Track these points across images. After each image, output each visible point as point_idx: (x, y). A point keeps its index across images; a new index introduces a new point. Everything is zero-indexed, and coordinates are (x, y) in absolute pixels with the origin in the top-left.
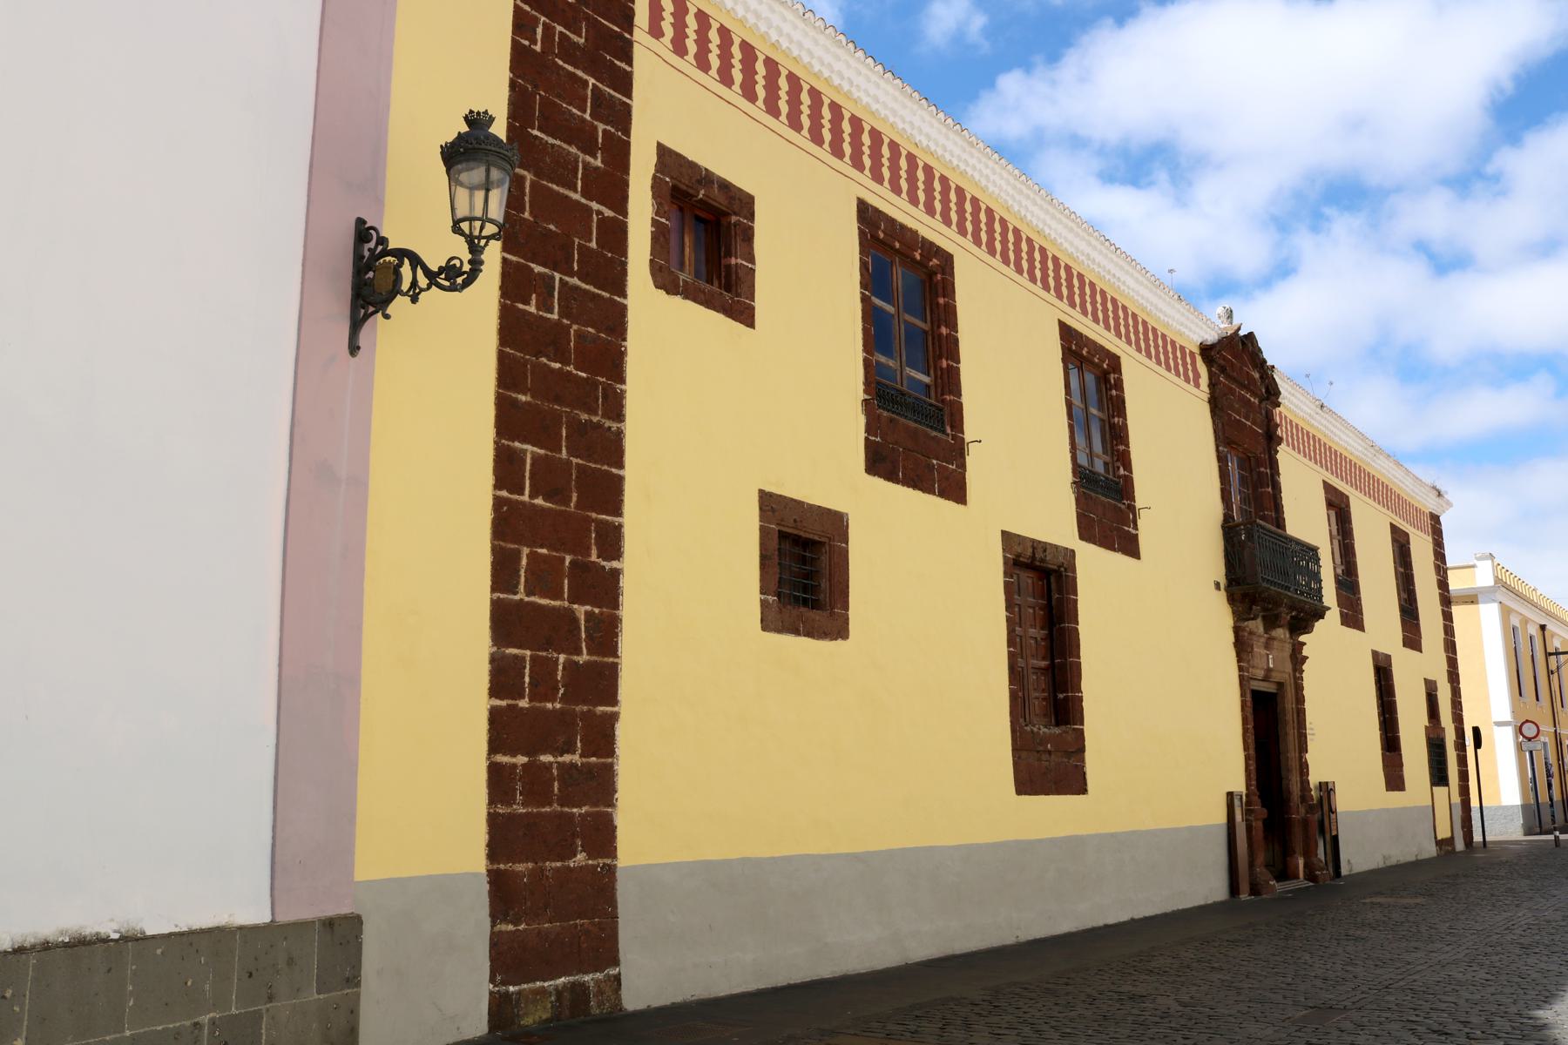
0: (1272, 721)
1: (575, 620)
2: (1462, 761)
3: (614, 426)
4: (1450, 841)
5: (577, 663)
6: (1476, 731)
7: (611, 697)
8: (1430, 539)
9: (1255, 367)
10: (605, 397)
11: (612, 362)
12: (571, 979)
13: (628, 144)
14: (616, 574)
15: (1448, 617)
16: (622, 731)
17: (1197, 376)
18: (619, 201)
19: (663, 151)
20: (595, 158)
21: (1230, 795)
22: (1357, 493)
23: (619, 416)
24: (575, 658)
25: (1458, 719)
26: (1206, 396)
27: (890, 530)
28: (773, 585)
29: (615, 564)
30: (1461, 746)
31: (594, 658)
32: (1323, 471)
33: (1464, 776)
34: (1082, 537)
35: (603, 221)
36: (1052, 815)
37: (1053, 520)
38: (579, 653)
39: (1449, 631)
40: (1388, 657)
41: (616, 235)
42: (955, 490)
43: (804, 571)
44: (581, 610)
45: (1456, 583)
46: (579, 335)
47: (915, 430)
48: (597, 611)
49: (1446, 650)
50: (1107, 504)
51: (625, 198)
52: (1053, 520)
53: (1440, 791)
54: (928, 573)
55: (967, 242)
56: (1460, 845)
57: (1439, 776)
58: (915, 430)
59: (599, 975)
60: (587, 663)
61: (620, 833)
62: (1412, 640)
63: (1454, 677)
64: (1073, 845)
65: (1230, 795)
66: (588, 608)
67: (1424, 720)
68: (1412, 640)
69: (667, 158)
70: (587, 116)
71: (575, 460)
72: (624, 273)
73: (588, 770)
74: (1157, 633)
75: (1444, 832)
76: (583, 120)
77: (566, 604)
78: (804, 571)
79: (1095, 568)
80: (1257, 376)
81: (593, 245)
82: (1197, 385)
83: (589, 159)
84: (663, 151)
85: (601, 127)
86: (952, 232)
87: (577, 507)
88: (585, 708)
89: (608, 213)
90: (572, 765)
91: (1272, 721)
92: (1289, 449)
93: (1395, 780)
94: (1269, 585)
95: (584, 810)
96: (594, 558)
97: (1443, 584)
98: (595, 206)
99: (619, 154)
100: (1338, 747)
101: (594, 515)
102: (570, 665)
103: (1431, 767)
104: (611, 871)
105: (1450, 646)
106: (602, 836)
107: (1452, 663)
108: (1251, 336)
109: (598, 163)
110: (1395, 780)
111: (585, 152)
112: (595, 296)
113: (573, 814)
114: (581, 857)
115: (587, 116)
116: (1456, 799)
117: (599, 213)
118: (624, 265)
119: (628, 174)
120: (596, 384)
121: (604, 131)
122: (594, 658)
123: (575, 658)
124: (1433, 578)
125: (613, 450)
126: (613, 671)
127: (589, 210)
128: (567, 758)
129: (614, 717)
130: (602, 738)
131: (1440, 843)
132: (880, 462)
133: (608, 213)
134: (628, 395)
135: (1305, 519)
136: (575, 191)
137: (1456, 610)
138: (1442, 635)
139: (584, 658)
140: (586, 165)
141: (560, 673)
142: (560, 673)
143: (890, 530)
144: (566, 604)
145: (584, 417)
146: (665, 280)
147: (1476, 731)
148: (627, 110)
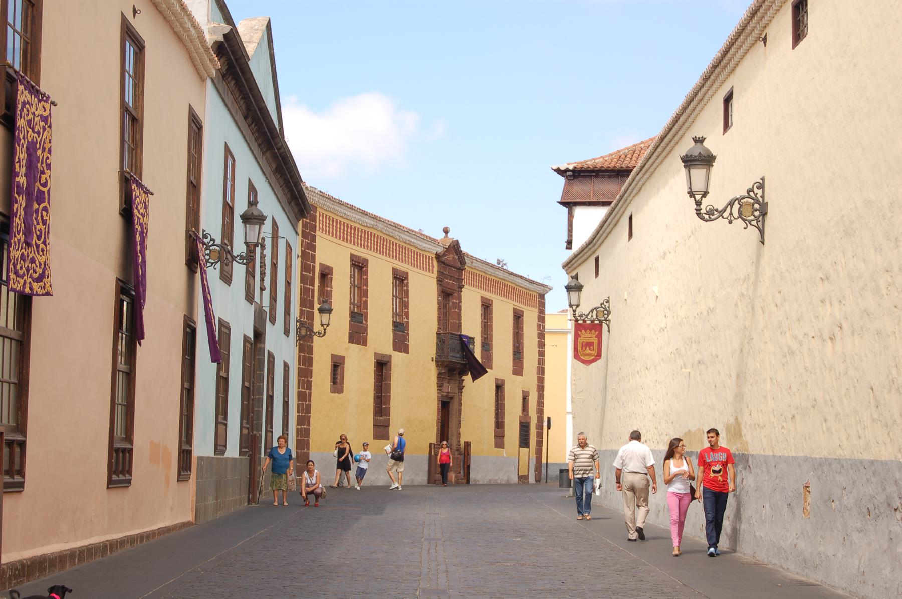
2: (540, 435)
6: (549, 419)
9: (457, 254)
15: (542, 345)
17: (433, 267)
21: (431, 444)
25: (540, 412)
26: (435, 275)
30: (540, 427)
32: (479, 291)
33: (539, 444)
37: (386, 348)
39: (541, 362)
40: (503, 381)
45: (549, 325)
49: (538, 373)
50: (401, 342)
52: (386, 348)
53: (524, 451)
56: (532, 480)
57: (524, 442)
62: (518, 370)
63: (541, 388)
65: (431, 444)
68: (518, 370)
69: (321, 264)
75: (523, 472)
79: (398, 359)
91: (448, 409)
103: (520, 438)
105: (541, 371)
107: (541, 381)
116: (533, 457)
124: (535, 332)
137: (548, 339)
138: (536, 365)
147: (549, 419)
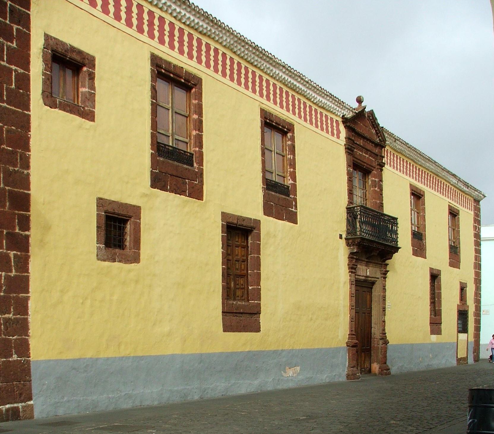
0: (365, 297)
1: (10, 258)
3: (26, 172)
4: (465, 359)
5: (10, 276)
7: (26, 290)
8: (472, 213)
10: (21, 159)
11: (23, 142)
12: (12, 405)
13: (29, 35)
14: (27, 237)
16: (31, 304)
17: (339, 132)
18: (25, 63)
19: (47, 37)
20: (12, 43)
22: (430, 190)
23: (28, 167)
24: (10, 274)
27: (163, 216)
28: (103, 239)
29: (27, 233)
31: (18, 274)
34: (265, 214)
35: (18, 75)
36: (241, 341)
37: (250, 204)
38: (11, 272)
41: (24, 81)
42: (197, 193)
43: (117, 230)
44: (12, 254)
46: (8, 131)
47: (177, 167)
48: (19, 253)
50: (280, 197)
51: (28, 63)
52: (250, 204)
53: (463, 336)
54: (181, 237)
55: (211, 72)
56: (471, 360)
57: (463, 328)
58: (177, 167)
59: (23, 404)
60: (15, 276)
61: (31, 347)
63: (478, 281)
64: (253, 356)
66: (15, 252)
67: (457, 301)
70: (8, 22)
71: (7, 188)
72: (29, 99)
73: (17, 320)
74: (306, 274)
75: (462, 354)
76: (6, 24)
77: (5, 251)
78: (117, 230)
79: (271, 228)
80: (374, 132)
81: (13, 86)
82: (338, 137)
83: (9, 43)
84: (47, 37)
85: (15, 27)
86: (203, 67)
87: (9, 208)
88: (15, 295)
89: (20, 71)
90: (10, 319)
92: (391, 169)
93: (436, 325)
94: (372, 243)
95: (15, 337)
96: (17, 231)
97: (477, 236)
98: (13, 67)
99: (25, 40)
100: (404, 316)
101: (17, 212)
102: (7, 278)
104: (28, 362)
105: (478, 266)
106: (24, 348)
108: (372, 113)
109: (14, 45)
110: (436, 325)
111: (7, 41)
112: (14, 112)
113: (11, 340)
114: (15, 357)
115: (8, 22)
116: (472, 339)
117: (16, 71)
118: (29, 96)
119: (29, 49)
120: (17, 152)
121: (17, 29)
122: (18, 274)
123: (10, 274)
125: (26, 182)
126: (27, 278)
127: (11, 70)
128: (7, 316)
129: (28, 298)
130: (22, 307)
131: (459, 360)
132: (158, 181)
133: (20, 71)
134: (31, 157)
135: (395, 200)
136: (4, 61)
139: (13, 273)
140: (9, 48)
141: (3, 281)
142: (3, 281)
143: (163, 216)
144: (5, 251)
145: (11, 168)
146: (50, 99)
148: (28, 17)
